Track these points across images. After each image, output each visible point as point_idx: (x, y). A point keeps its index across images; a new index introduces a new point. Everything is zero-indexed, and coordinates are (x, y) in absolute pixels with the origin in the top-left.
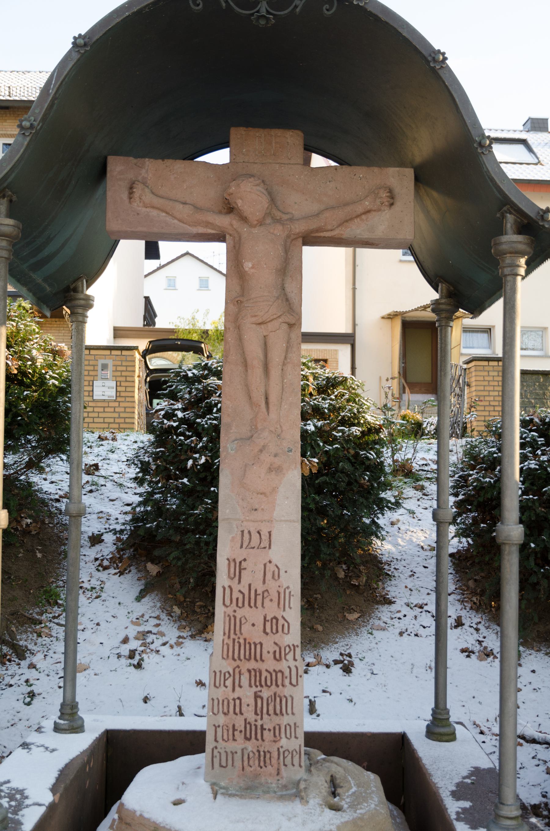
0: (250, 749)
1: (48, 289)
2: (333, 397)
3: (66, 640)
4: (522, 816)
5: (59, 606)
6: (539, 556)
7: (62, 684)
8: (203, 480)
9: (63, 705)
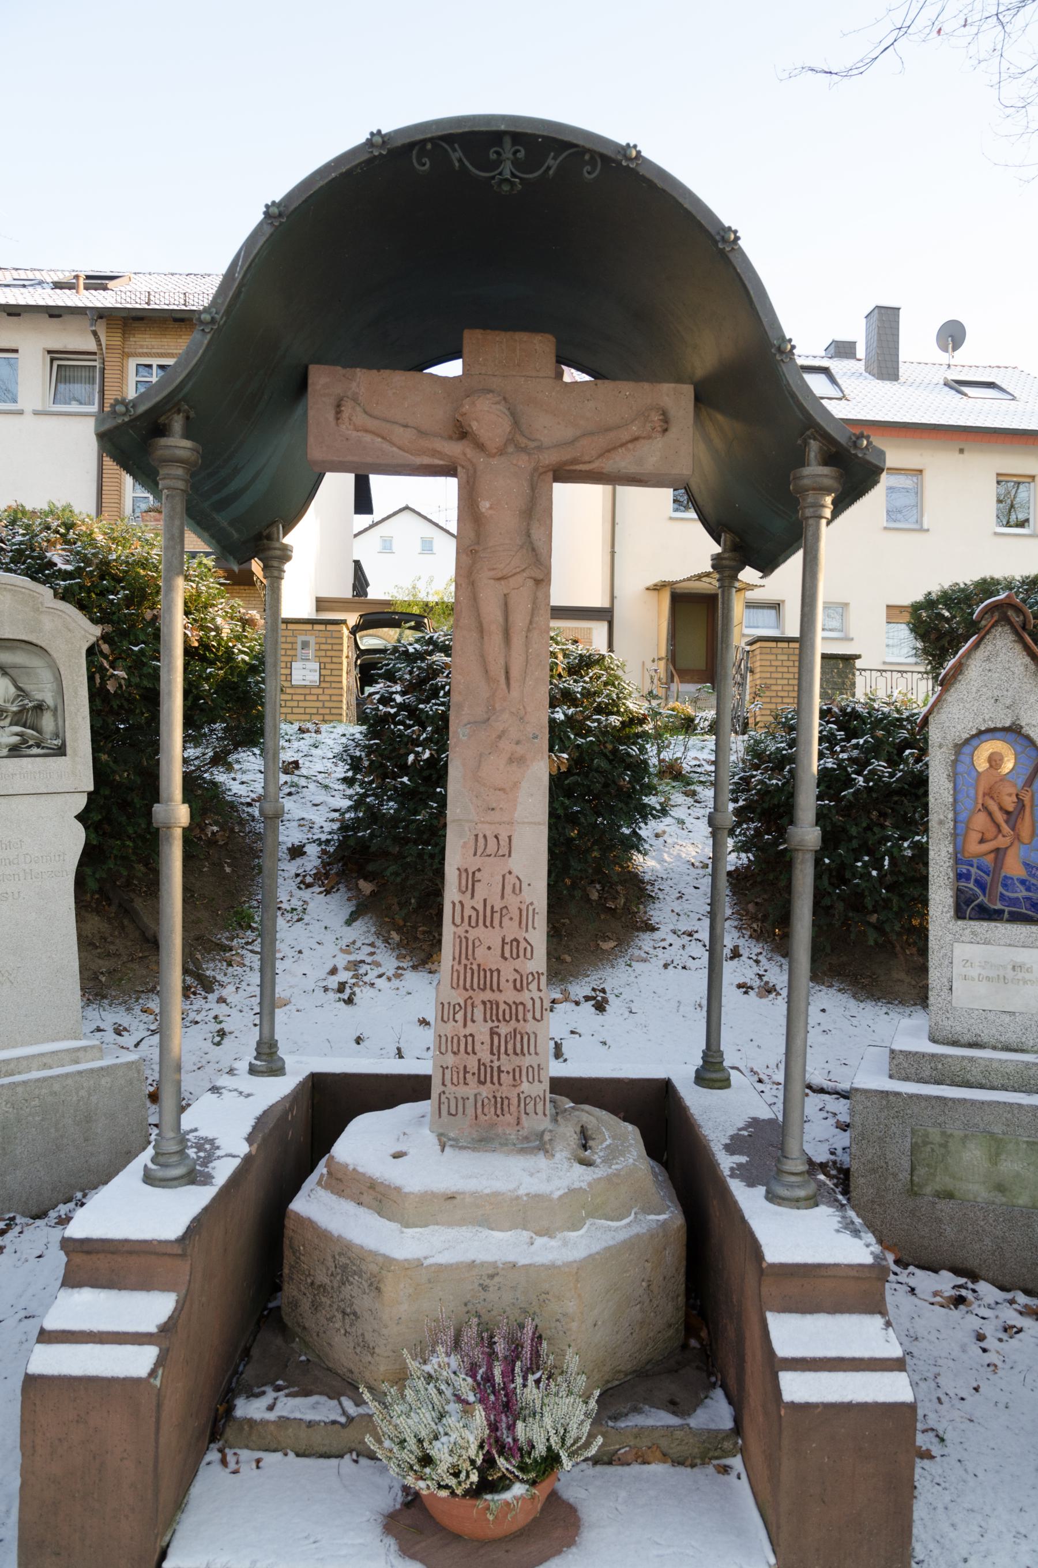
0: (484, 1094)
1: (236, 535)
2: (587, 679)
3: (261, 970)
4: (808, 1172)
5: (253, 930)
6: (834, 874)
7: (257, 1022)
8: (427, 780)
9: (259, 1043)
